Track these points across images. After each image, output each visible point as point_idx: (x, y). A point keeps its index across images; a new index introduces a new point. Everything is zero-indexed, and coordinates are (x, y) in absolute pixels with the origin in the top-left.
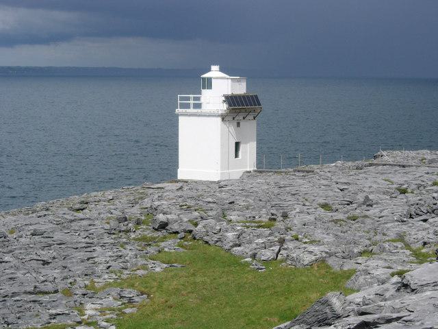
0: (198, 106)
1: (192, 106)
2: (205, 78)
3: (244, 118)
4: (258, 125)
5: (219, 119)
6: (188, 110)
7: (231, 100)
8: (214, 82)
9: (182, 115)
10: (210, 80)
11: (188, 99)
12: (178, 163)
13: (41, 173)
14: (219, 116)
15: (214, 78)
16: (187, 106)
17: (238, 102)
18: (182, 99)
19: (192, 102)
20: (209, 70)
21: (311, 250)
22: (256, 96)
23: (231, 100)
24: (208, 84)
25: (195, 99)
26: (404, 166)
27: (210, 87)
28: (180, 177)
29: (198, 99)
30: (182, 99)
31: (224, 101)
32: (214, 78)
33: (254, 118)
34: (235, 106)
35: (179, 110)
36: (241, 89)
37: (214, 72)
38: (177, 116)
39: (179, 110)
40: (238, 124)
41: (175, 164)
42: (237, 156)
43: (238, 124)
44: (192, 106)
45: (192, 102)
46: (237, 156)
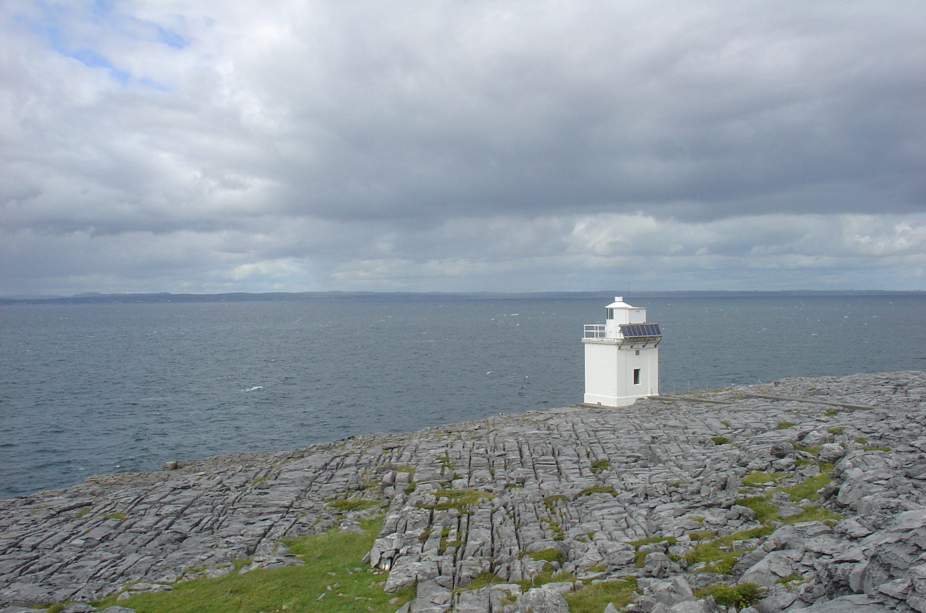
0: (603, 335)
5: (616, 347)
7: (626, 330)
10: (612, 310)
13: (672, 490)
16: (592, 335)
17: (644, 331)
18: (588, 328)
20: (613, 301)
23: (626, 330)
24: (610, 314)
26: (43, 451)
27: (612, 318)
28: (587, 400)
29: (604, 328)
30: (588, 328)
35: (585, 339)
36: (640, 318)
37: (618, 303)
39: (585, 339)
40: (637, 353)
41: (583, 391)
42: (636, 381)
43: (637, 353)
46: (636, 381)
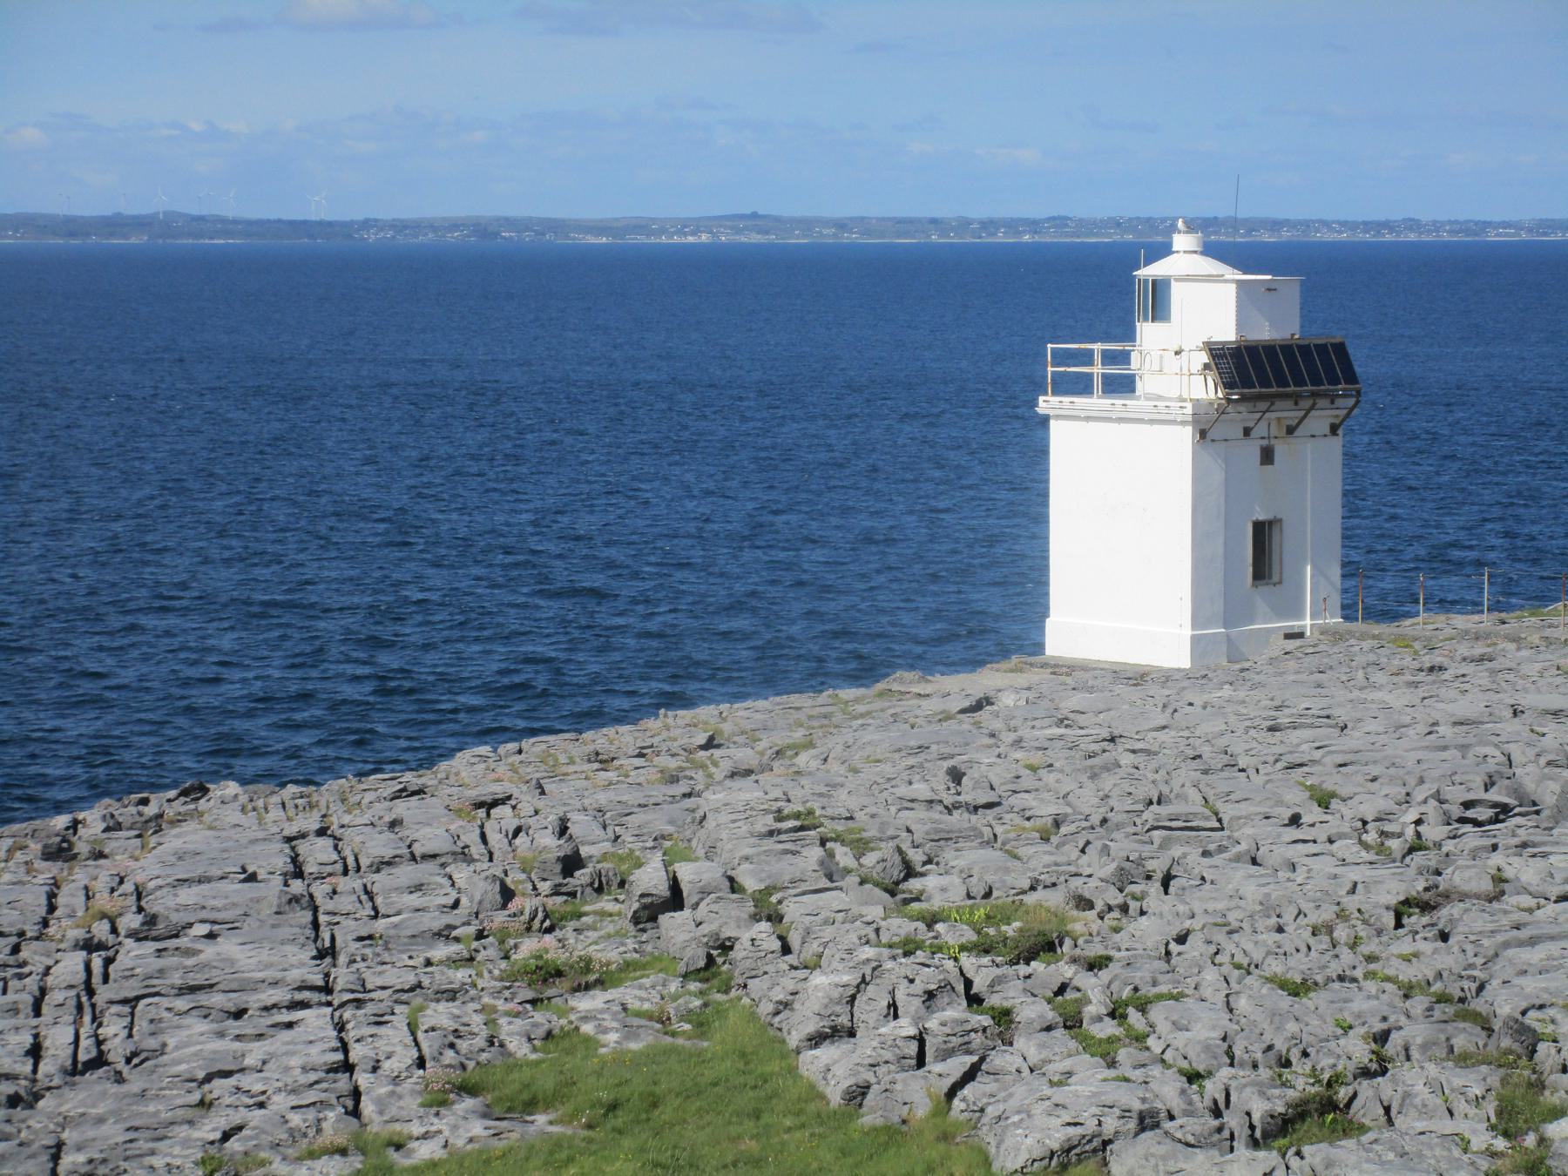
0: (1122, 385)
1: (1097, 384)
2: (1146, 281)
3: (1291, 430)
4: (1349, 457)
6: (1080, 401)
8: (1179, 294)
9: (1058, 417)
10: (1159, 288)
11: (1087, 358)
12: (1046, 558)
14: (1183, 423)
15: (1180, 279)
16: (1081, 386)
18: (1062, 358)
19: (1097, 370)
20: (1164, 250)
21: (723, 627)
22: (1340, 349)
25: (1109, 358)
29: (1123, 358)
30: (1062, 358)
31: (1206, 367)
32: (1180, 279)
33: (1334, 429)
34: (1265, 383)
38: (1044, 421)
43: (1267, 456)
44: (1097, 384)
45: (1097, 370)
